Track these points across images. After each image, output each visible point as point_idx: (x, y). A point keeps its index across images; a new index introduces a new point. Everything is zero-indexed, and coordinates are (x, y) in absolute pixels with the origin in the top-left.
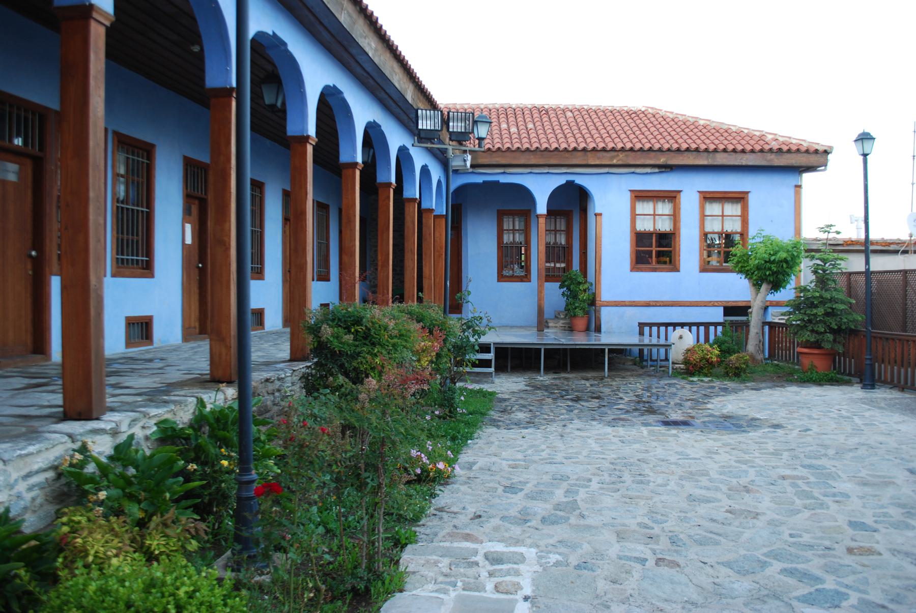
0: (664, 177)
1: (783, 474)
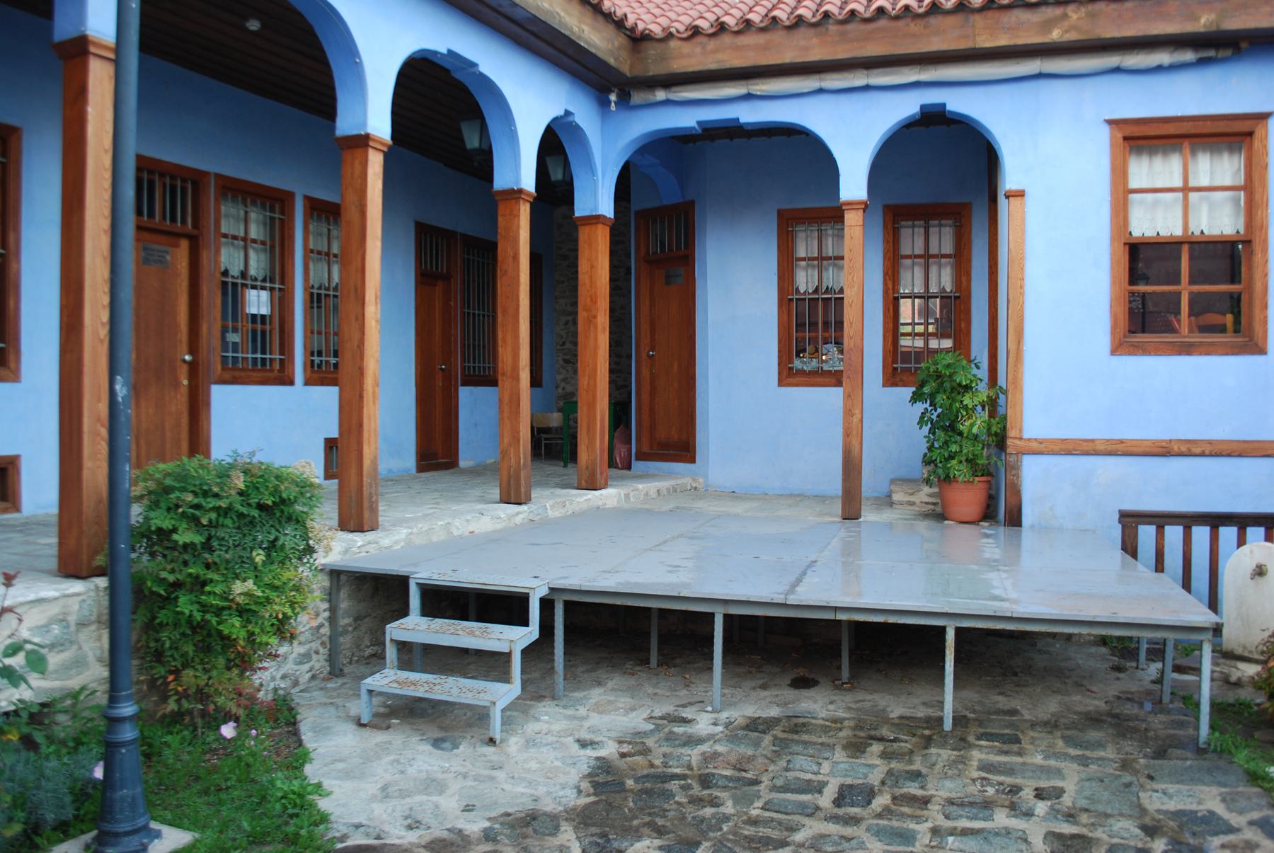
0: (1212, 75)
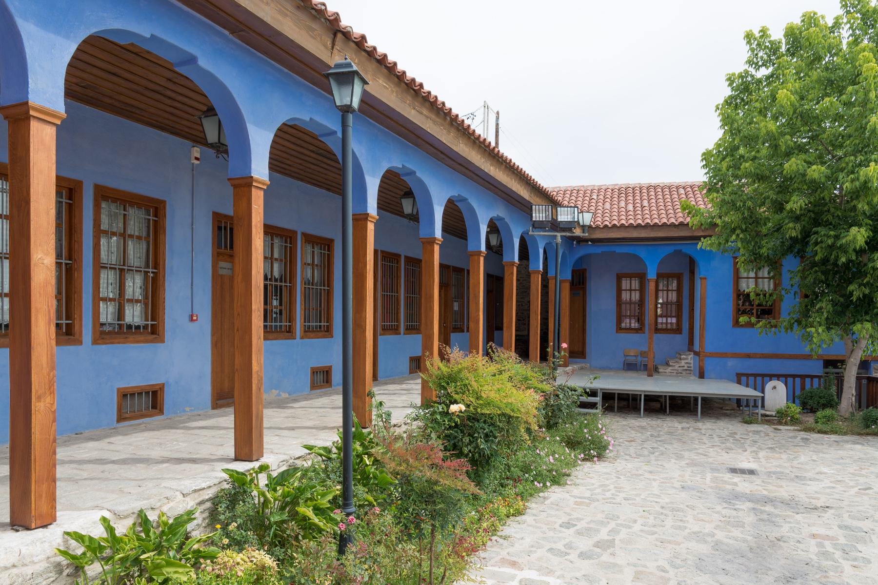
1: (814, 532)
